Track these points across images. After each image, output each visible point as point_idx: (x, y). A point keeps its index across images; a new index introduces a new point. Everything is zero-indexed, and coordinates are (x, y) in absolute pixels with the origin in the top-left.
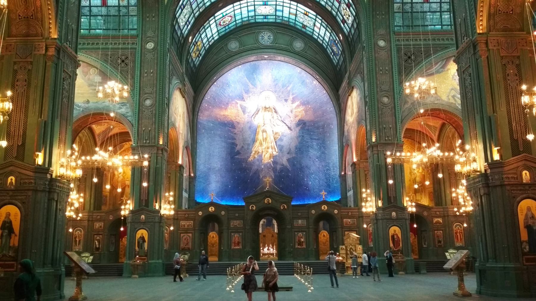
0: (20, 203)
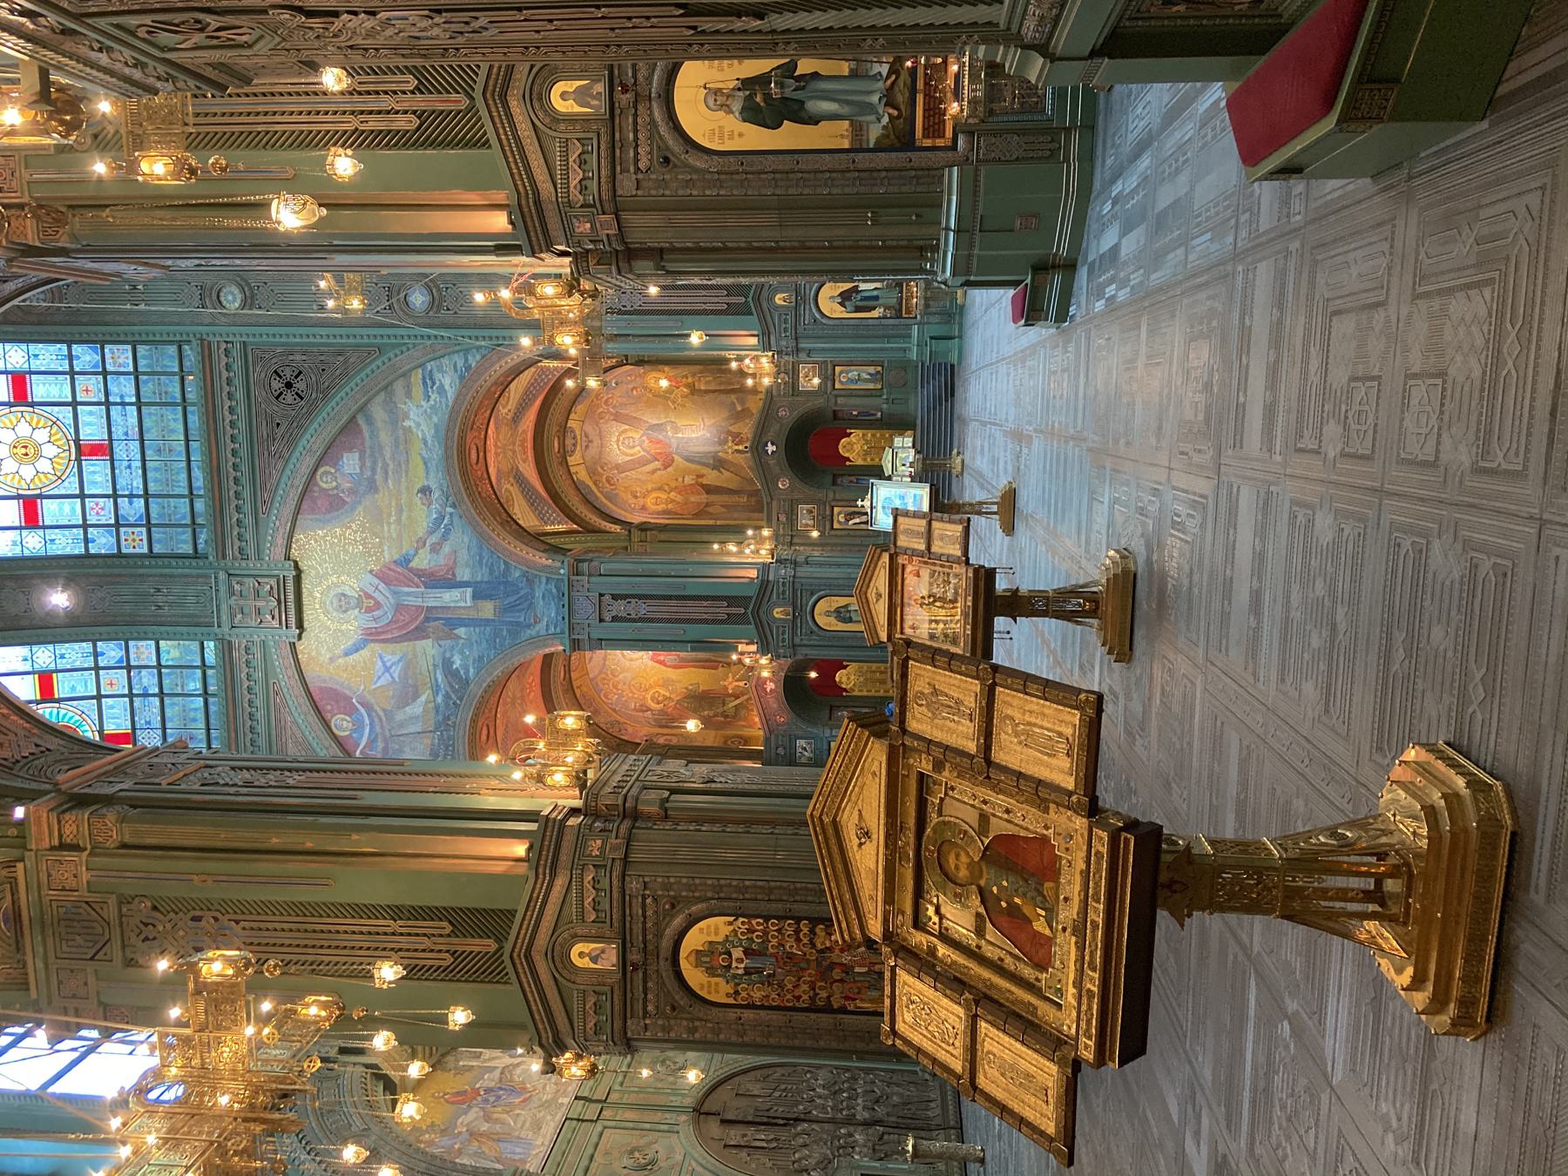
0: (673, 917)
